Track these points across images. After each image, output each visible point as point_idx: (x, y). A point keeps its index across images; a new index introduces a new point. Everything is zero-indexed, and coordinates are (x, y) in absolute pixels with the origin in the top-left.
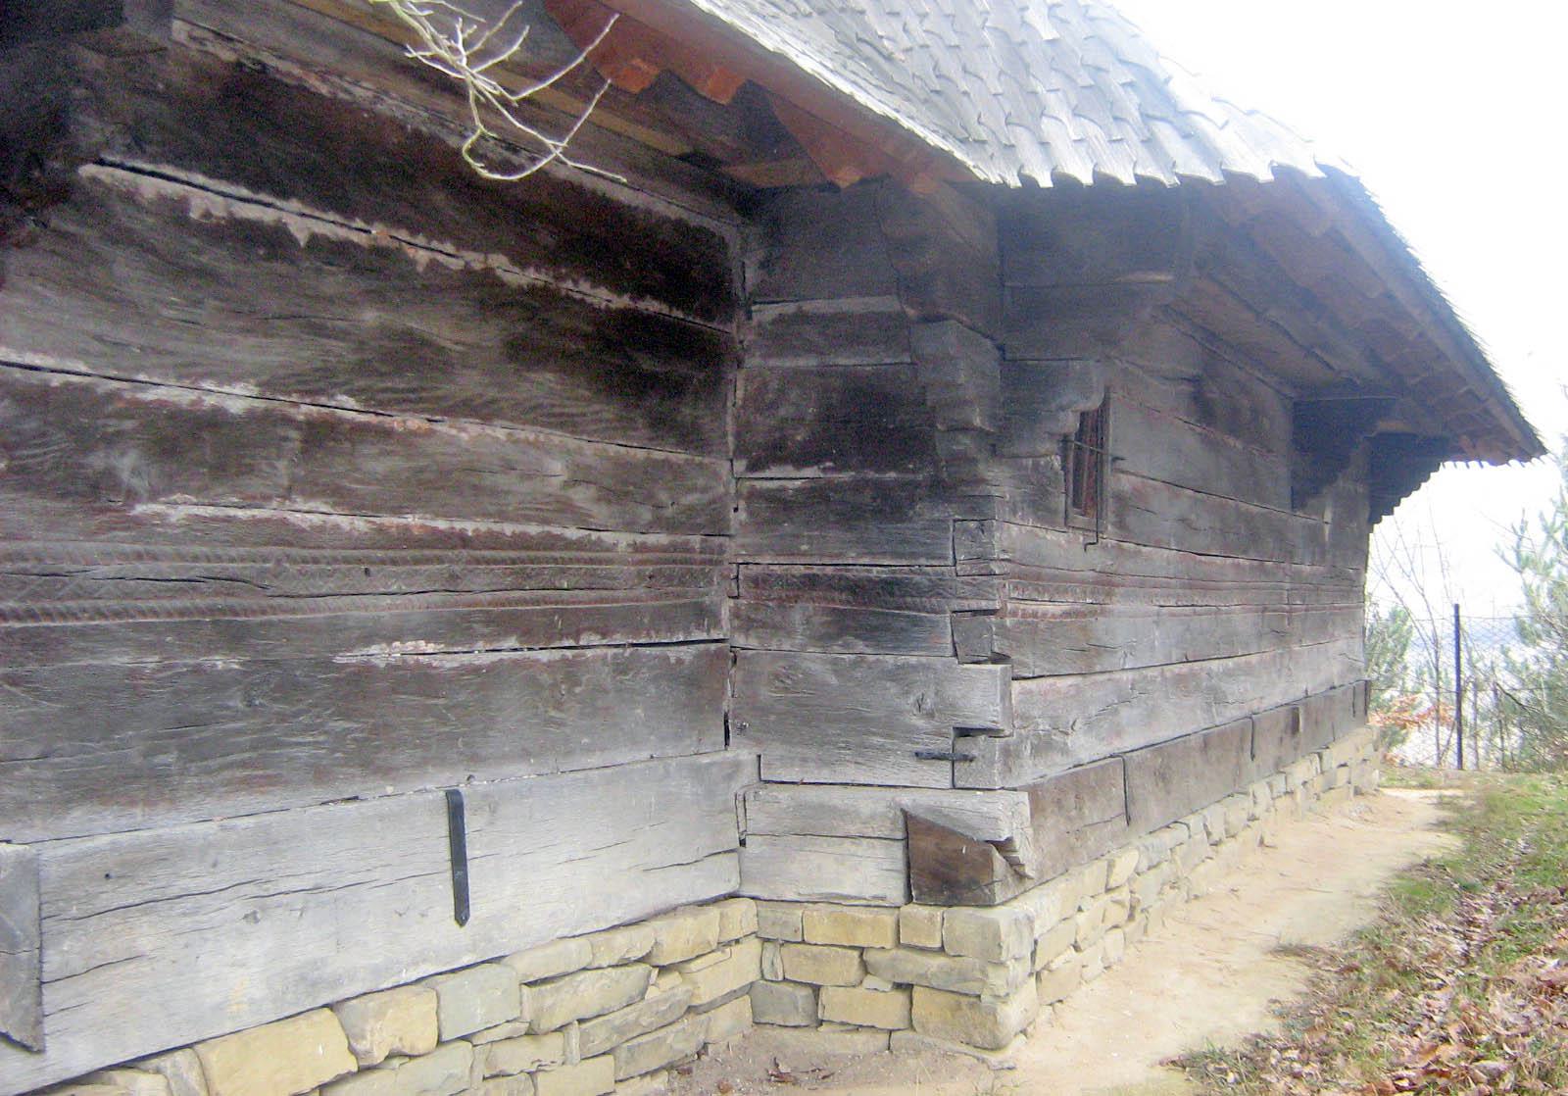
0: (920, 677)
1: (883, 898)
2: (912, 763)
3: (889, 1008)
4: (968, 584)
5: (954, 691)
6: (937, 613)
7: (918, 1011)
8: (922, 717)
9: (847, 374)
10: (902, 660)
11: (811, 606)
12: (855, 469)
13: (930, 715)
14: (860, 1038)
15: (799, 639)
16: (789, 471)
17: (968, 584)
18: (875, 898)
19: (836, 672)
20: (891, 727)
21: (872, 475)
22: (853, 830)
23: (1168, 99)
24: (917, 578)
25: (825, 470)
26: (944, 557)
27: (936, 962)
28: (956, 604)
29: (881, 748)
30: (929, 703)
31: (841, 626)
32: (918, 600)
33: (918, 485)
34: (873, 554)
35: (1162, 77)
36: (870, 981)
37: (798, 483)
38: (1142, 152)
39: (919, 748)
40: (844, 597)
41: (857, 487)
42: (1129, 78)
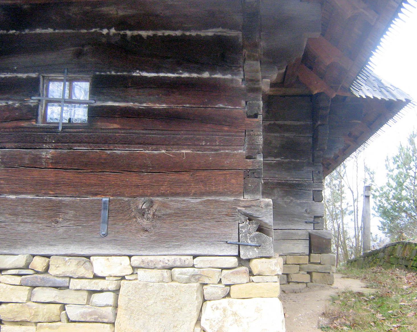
0: (306, 205)
1: (304, 253)
2: (305, 224)
3: (306, 278)
4: (317, 185)
5: (314, 208)
6: (309, 191)
7: (314, 278)
8: (307, 214)
9: (288, 138)
10: (301, 201)
11: (278, 189)
12: (289, 159)
13: (309, 213)
14: (300, 285)
15: (276, 197)
16: (273, 159)
17: (317, 185)
18: (303, 253)
19: (286, 204)
20: (300, 216)
21: (293, 160)
22: (297, 238)
23: (382, 84)
24: (305, 183)
25: (282, 159)
26: (310, 179)
27: (318, 266)
28: (314, 189)
29: (297, 221)
30: (308, 211)
31: (287, 193)
32: (305, 188)
33: (303, 163)
34: (294, 178)
35: (380, 79)
36: (301, 272)
37: (275, 161)
38: (380, 94)
39: (307, 221)
40: (287, 187)
41: (289, 163)
42: (374, 79)
